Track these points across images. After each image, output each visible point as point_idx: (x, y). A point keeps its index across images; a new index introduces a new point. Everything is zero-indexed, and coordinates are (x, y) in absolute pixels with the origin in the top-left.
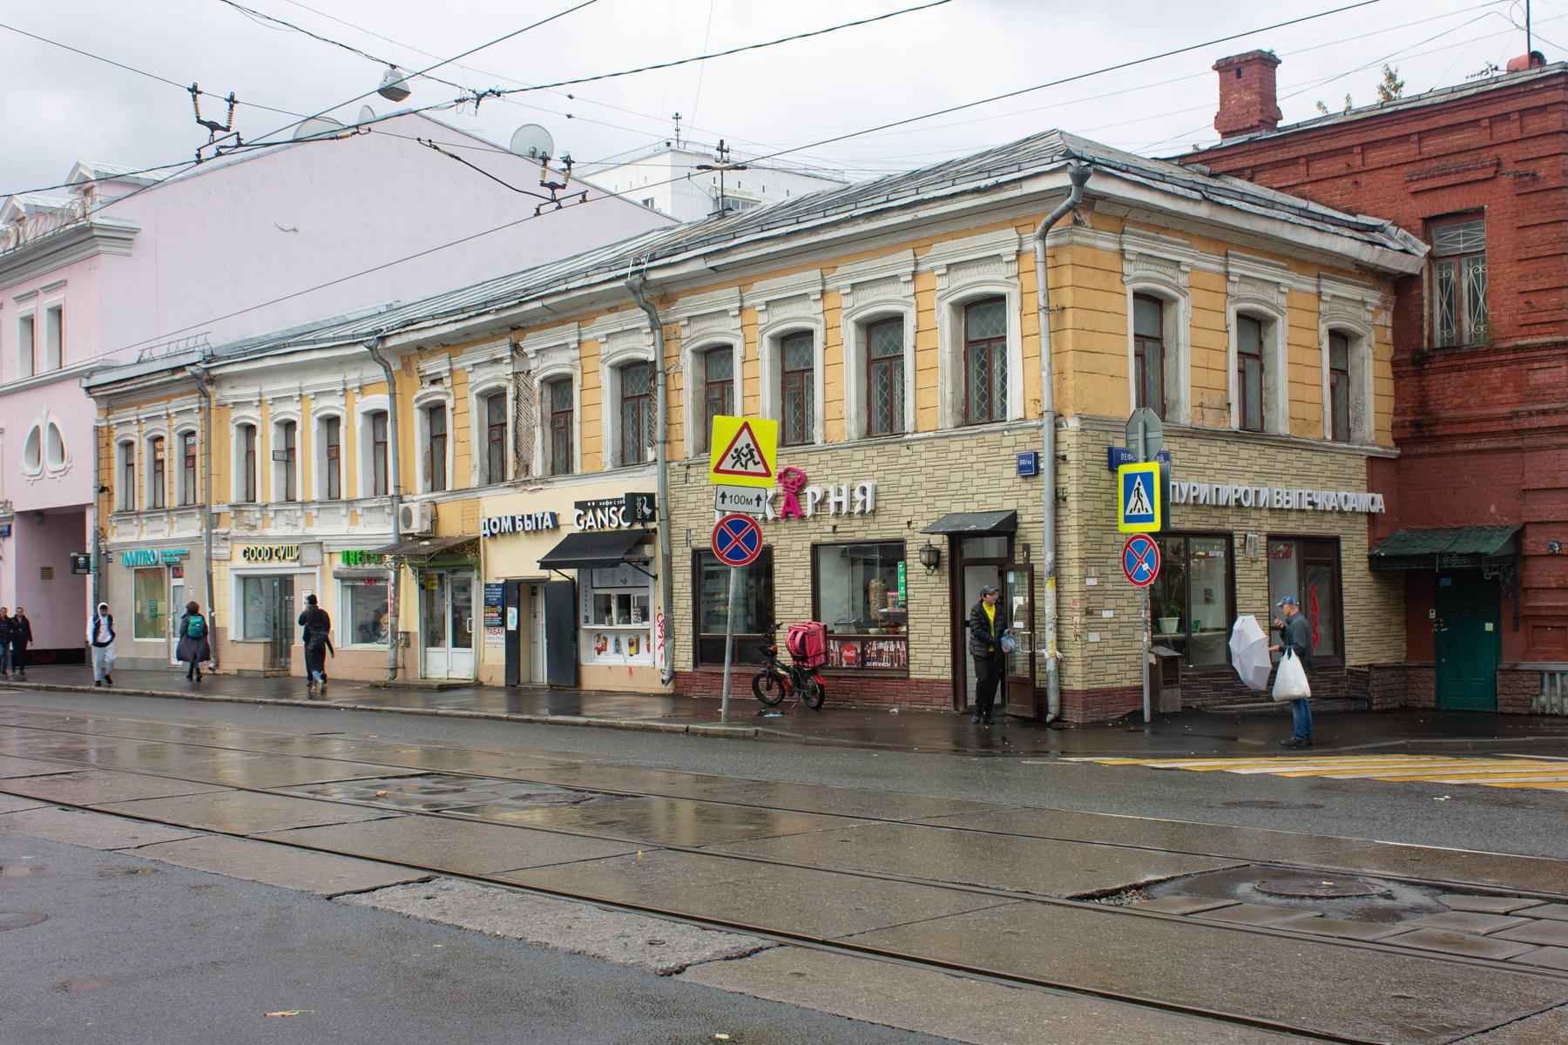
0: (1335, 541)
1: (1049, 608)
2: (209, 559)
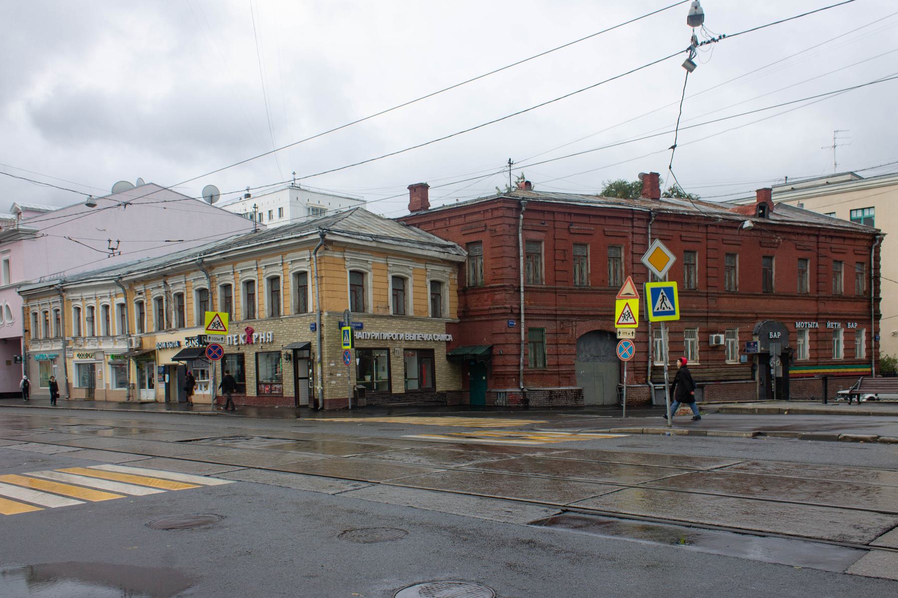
0: (433, 350)
1: (319, 373)
2: (65, 357)
